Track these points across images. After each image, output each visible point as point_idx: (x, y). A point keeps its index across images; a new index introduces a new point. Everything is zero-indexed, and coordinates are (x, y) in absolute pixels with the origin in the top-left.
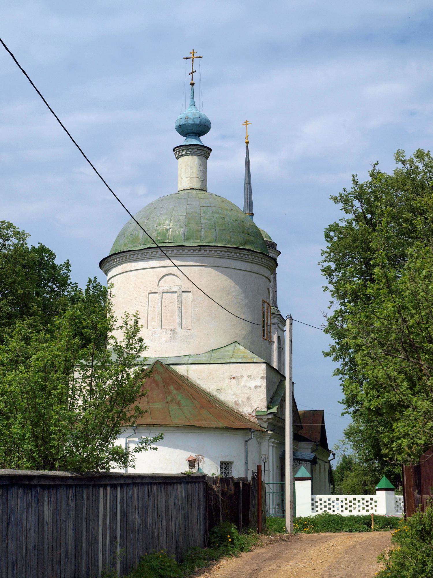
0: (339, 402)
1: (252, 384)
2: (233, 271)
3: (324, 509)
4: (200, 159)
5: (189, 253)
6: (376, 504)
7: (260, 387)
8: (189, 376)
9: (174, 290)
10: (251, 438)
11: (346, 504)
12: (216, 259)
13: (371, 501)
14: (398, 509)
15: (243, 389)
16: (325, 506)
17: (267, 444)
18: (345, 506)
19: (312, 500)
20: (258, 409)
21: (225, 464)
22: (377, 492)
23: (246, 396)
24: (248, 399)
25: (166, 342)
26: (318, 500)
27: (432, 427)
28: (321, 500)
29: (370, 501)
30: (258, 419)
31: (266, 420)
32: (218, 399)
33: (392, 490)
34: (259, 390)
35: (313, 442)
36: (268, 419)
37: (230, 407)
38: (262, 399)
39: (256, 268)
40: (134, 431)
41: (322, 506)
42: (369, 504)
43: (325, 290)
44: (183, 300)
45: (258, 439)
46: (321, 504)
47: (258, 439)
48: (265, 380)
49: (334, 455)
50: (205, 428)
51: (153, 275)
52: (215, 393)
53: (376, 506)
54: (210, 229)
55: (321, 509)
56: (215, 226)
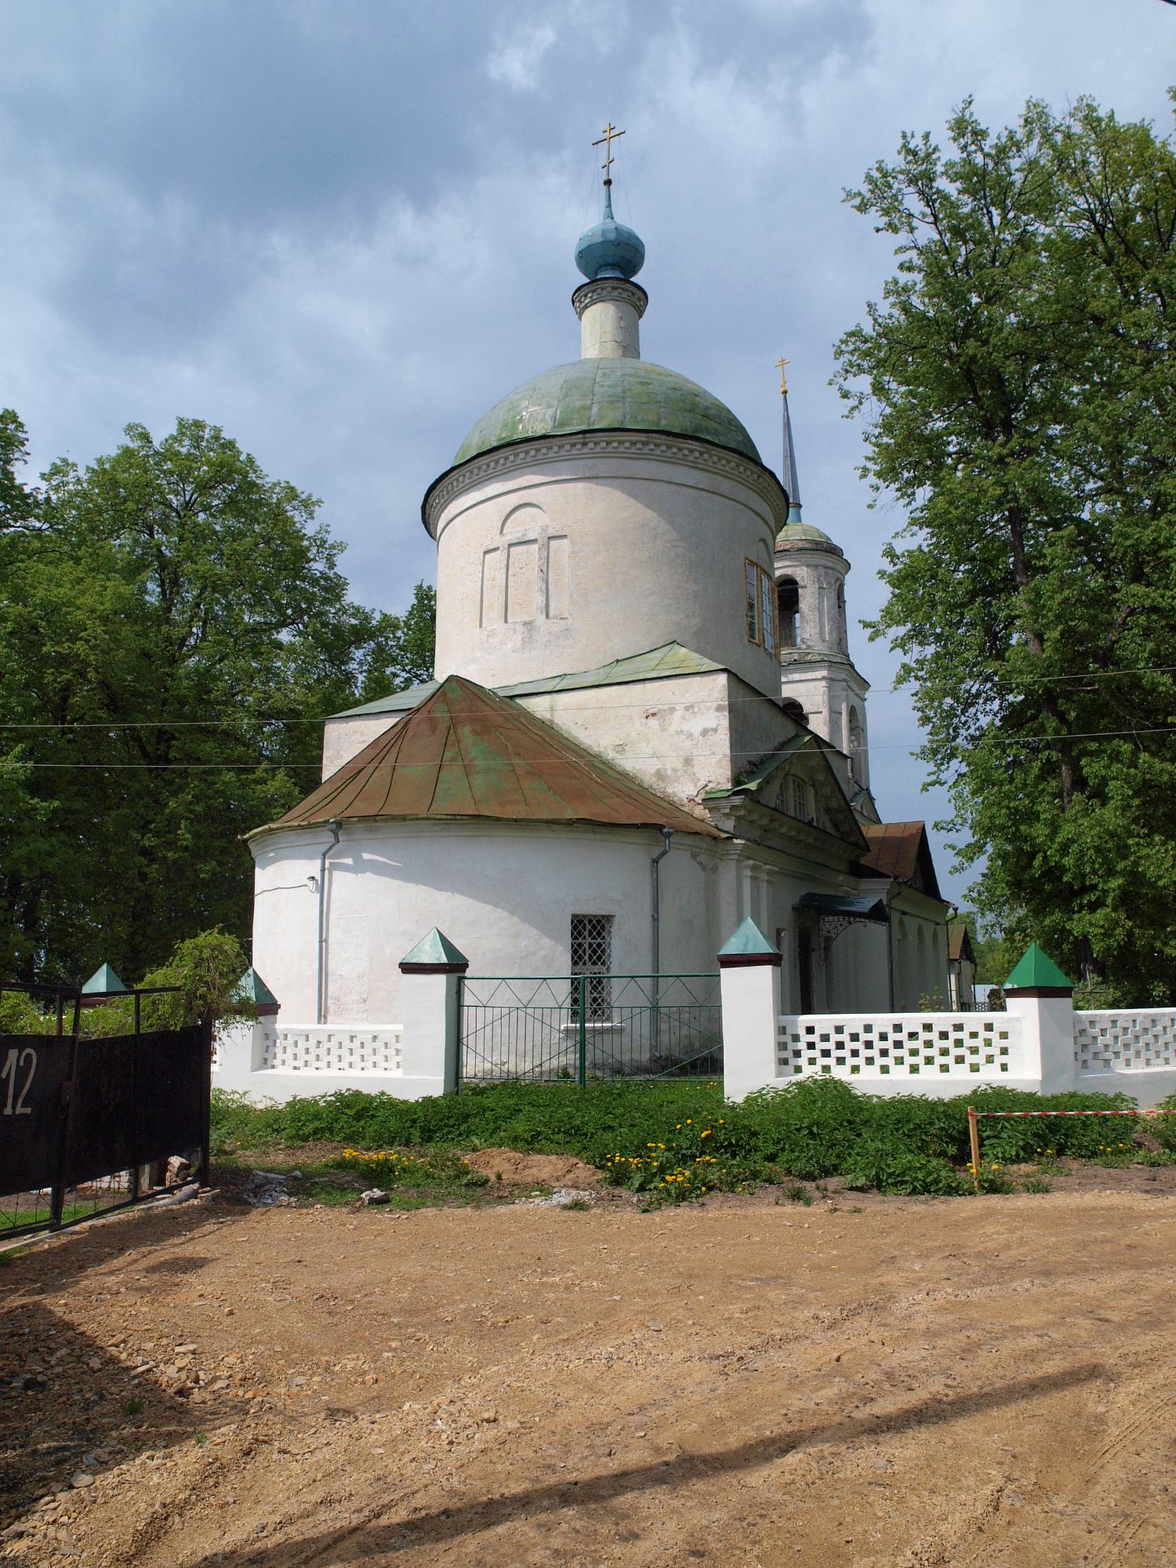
0: (912, 754)
1: (696, 725)
3: (823, 1061)
5: (563, 453)
6: (1004, 1043)
7: (715, 730)
8: (556, 721)
10: (665, 853)
13: (988, 1035)
14: (1088, 1056)
15: (677, 739)
16: (826, 1053)
17: (733, 871)
19: (782, 1030)
20: (711, 785)
21: (599, 922)
22: (1010, 1002)
24: (688, 761)
25: (515, 651)
26: (802, 1032)
27: (485, 1565)
28: (810, 1030)
29: (984, 1035)
30: (710, 810)
33: (1064, 992)
36: (733, 808)
38: (720, 761)
39: (725, 486)
40: (336, 835)
41: (816, 1053)
42: (978, 1043)
43: (863, 476)
44: (552, 555)
45: (702, 858)
46: (811, 1046)
47: (702, 858)
48: (726, 713)
50: (516, 820)
51: (493, 512)
52: (610, 755)
54: (612, 402)
55: (812, 1061)
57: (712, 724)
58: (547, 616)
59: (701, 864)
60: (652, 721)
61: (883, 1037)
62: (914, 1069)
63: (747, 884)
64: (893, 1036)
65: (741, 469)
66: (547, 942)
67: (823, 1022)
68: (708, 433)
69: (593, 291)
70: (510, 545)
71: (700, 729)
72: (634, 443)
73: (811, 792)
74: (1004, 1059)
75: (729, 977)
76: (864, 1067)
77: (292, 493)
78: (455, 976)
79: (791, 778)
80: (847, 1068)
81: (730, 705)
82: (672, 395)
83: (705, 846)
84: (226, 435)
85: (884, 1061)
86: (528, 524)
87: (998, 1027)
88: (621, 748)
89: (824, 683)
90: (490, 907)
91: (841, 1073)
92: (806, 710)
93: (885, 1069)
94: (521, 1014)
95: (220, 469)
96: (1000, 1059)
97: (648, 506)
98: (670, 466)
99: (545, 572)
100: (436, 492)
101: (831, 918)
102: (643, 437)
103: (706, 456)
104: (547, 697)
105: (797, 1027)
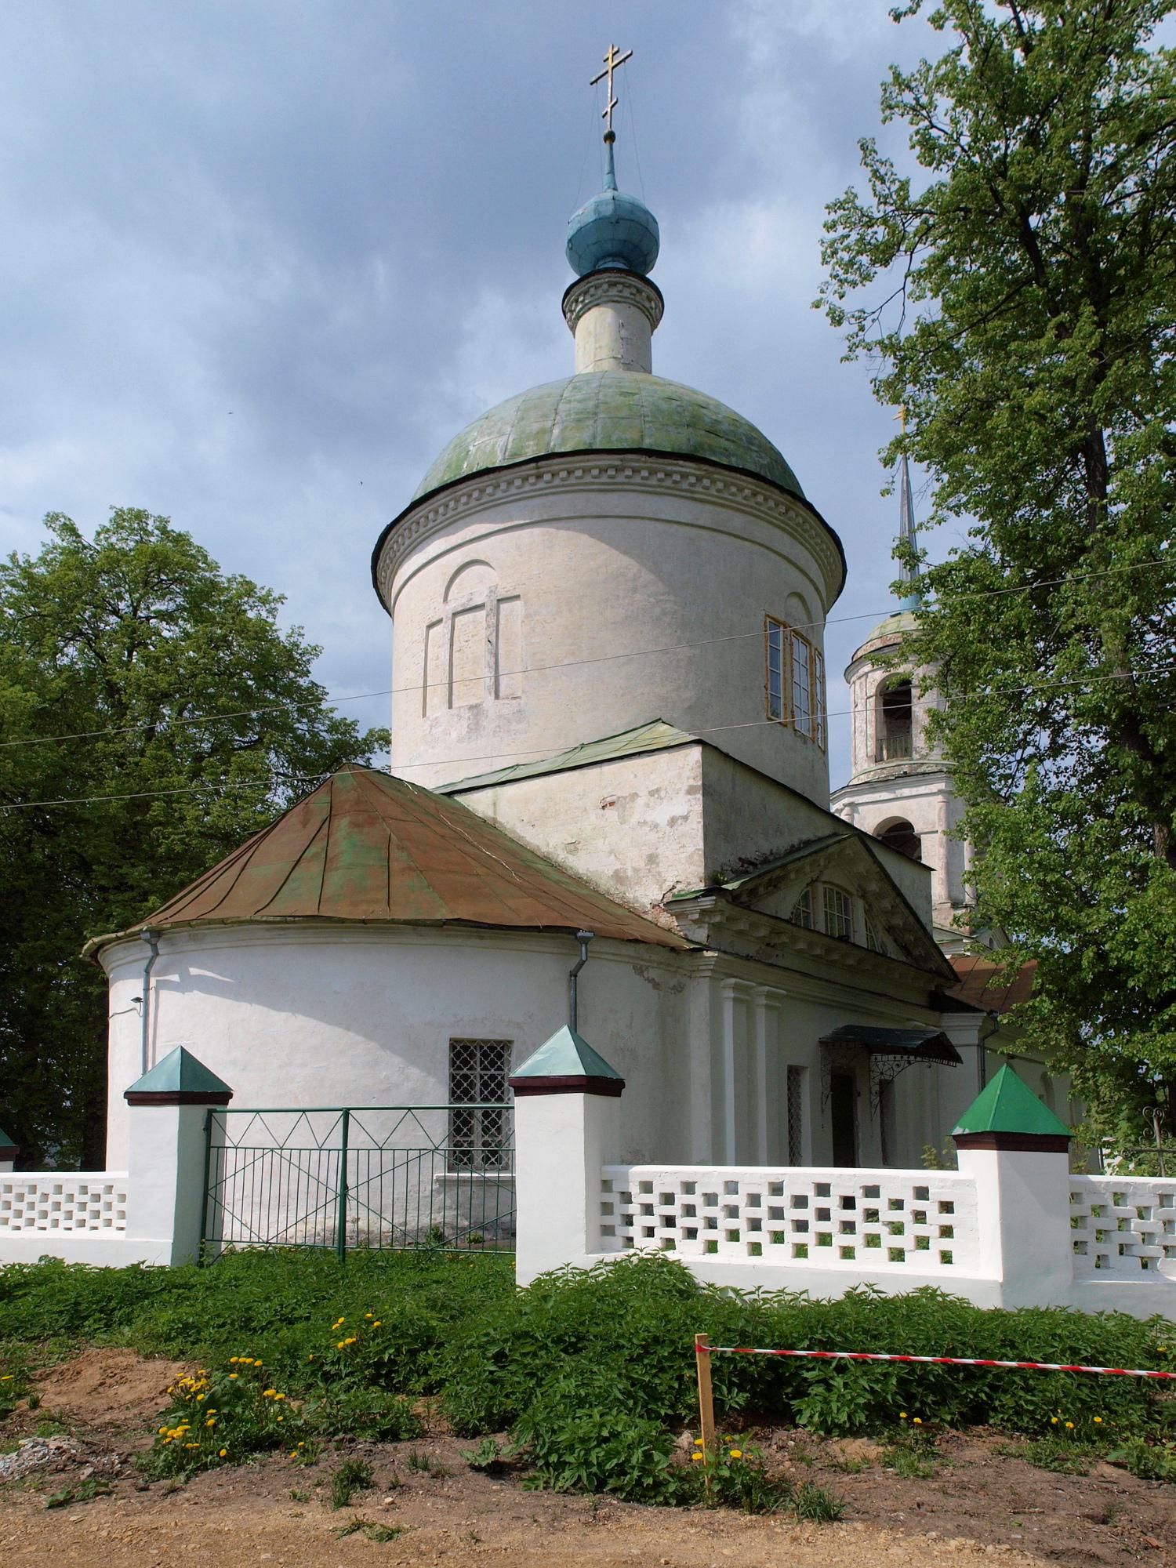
1: (662, 813)
2: (652, 525)
3: (663, 1232)
4: (618, 313)
5: (513, 491)
7: (685, 818)
10: (582, 964)
11: (777, 1213)
12: (593, 495)
13: (920, 1205)
18: (769, 1225)
19: (606, 1185)
20: (679, 887)
22: (963, 1155)
23: (647, 851)
24: (652, 859)
25: (460, 740)
28: (647, 1187)
30: (678, 916)
31: (697, 916)
32: (570, 872)
34: (681, 828)
35: (981, 1011)
36: (703, 912)
37: (602, 889)
38: (691, 856)
39: (737, 521)
42: (904, 1216)
44: (502, 622)
46: (648, 1209)
48: (700, 796)
50: (364, 921)
52: (560, 856)
53: (947, 1232)
54: (579, 420)
56: (596, 414)
57: (680, 811)
58: (497, 696)
59: (651, 981)
60: (609, 811)
61: (754, 1200)
62: (801, 1251)
63: (728, 1009)
64: (768, 1201)
65: (760, 498)
66: (414, 1072)
67: (666, 1176)
68: (715, 453)
69: (585, 293)
70: (455, 614)
71: (667, 817)
72: (603, 470)
73: (859, 906)
74: (946, 1244)
75: (526, 1111)
76: (724, 1245)
77: (249, 589)
78: (199, 1111)
79: (820, 887)
80: (698, 1244)
81: (704, 784)
82: (665, 406)
83: (655, 957)
84: (175, 526)
85: (755, 1237)
86: (475, 586)
87: (936, 1194)
88: (573, 847)
89: (940, 798)
90: (339, 1031)
91: (688, 1254)
92: (917, 829)
93: (756, 1249)
94: (276, 1158)
95: (163, 563)
96: (938, 1244)
97: (625, 553)
98: (656, 498)
99: (494, 643)
100: (381, 563)
101: (885, 1058)
102: (614, 460)
103: (706, 482)
104: (489, 792)
105: (627, 1182)
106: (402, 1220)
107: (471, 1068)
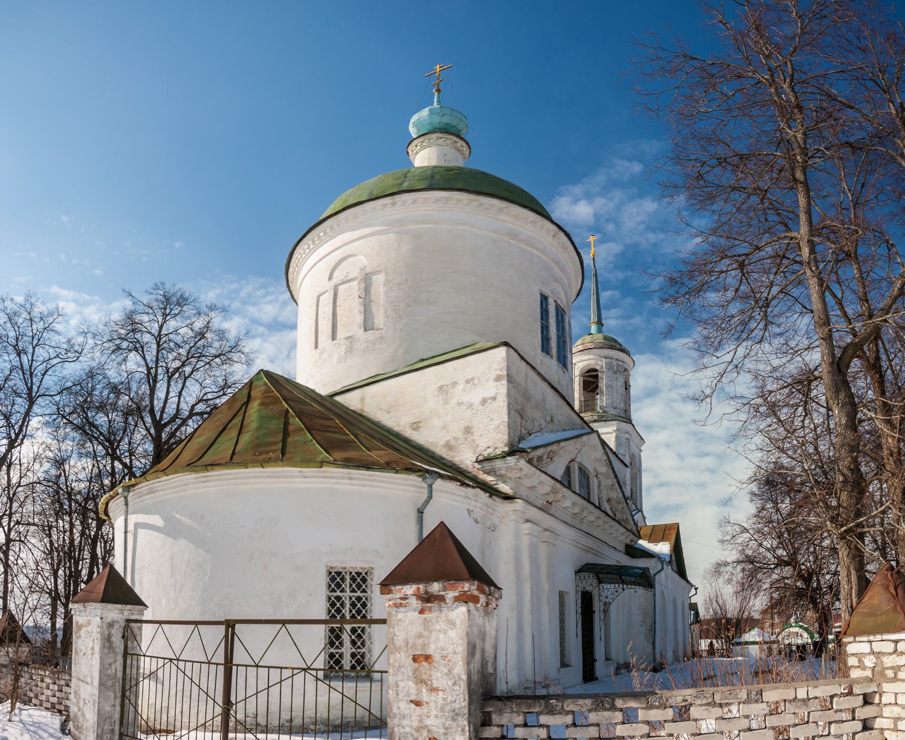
1: (475, 397)
7: (494, 399)
9: (351, 276)
22: (666, 725)
23: (464, 424)
24: (468, 430)
34: (490, 405)
38: (499, 426)
48: (505, 382)
49: (696, 589)
52: (408, 433)
88: (416, 426)
101: (609, 586)
106: (289, 718)
107: (343, 591)
